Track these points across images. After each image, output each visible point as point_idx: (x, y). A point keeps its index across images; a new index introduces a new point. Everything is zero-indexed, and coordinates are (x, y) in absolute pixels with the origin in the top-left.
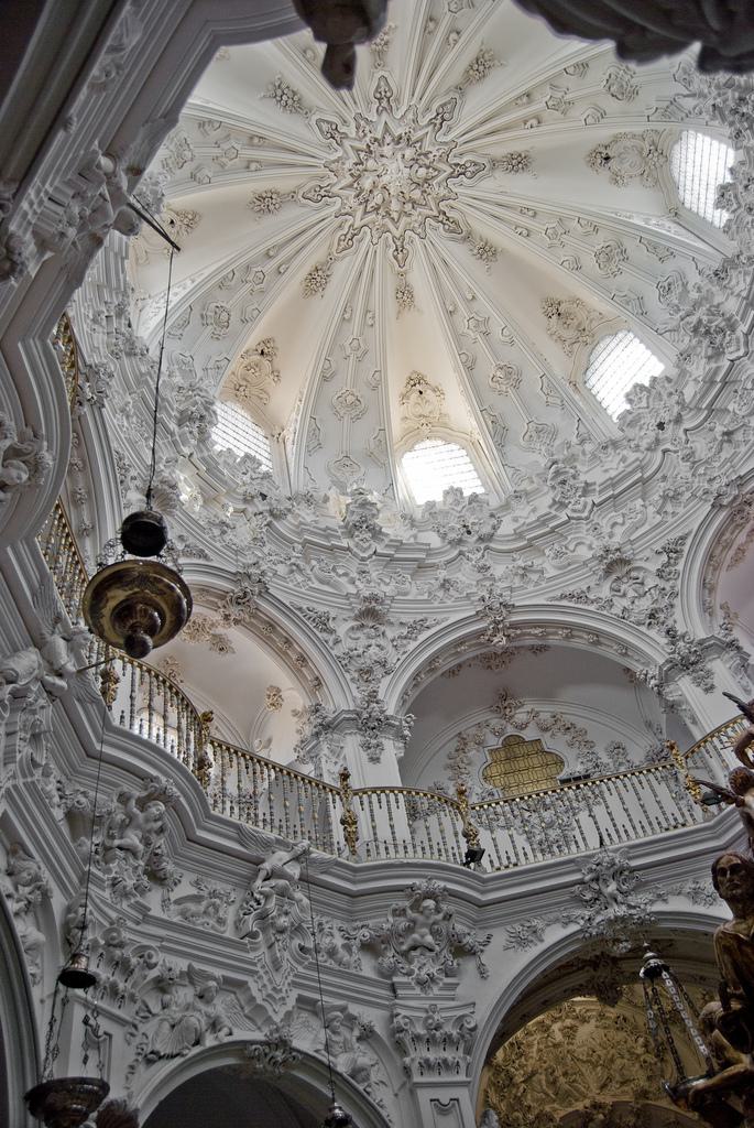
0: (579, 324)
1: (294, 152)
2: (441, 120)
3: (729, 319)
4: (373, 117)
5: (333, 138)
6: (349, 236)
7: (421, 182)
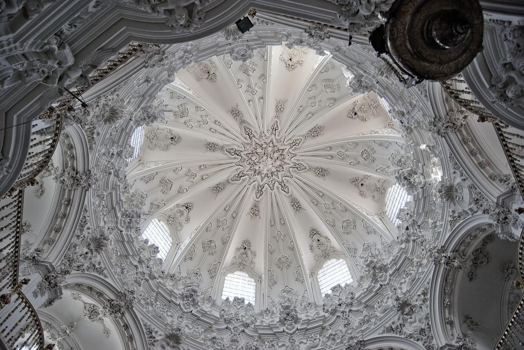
2: (239, 176)
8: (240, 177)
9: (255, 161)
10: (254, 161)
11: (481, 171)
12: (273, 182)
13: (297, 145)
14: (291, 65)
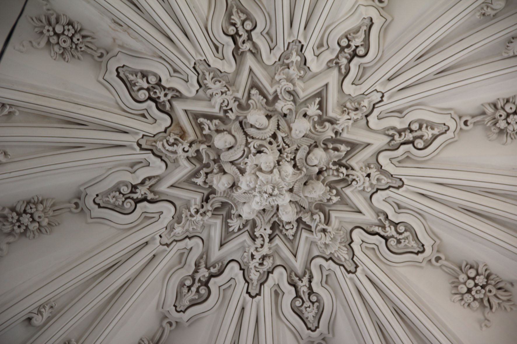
1: (81, 124)
5: (310, 288)
7: (235, 127)
8: (137, 201)
9: (226, 157)
10: (218, 152)
11: (151, 134)
12: (268, 264)
13: (420, 143)
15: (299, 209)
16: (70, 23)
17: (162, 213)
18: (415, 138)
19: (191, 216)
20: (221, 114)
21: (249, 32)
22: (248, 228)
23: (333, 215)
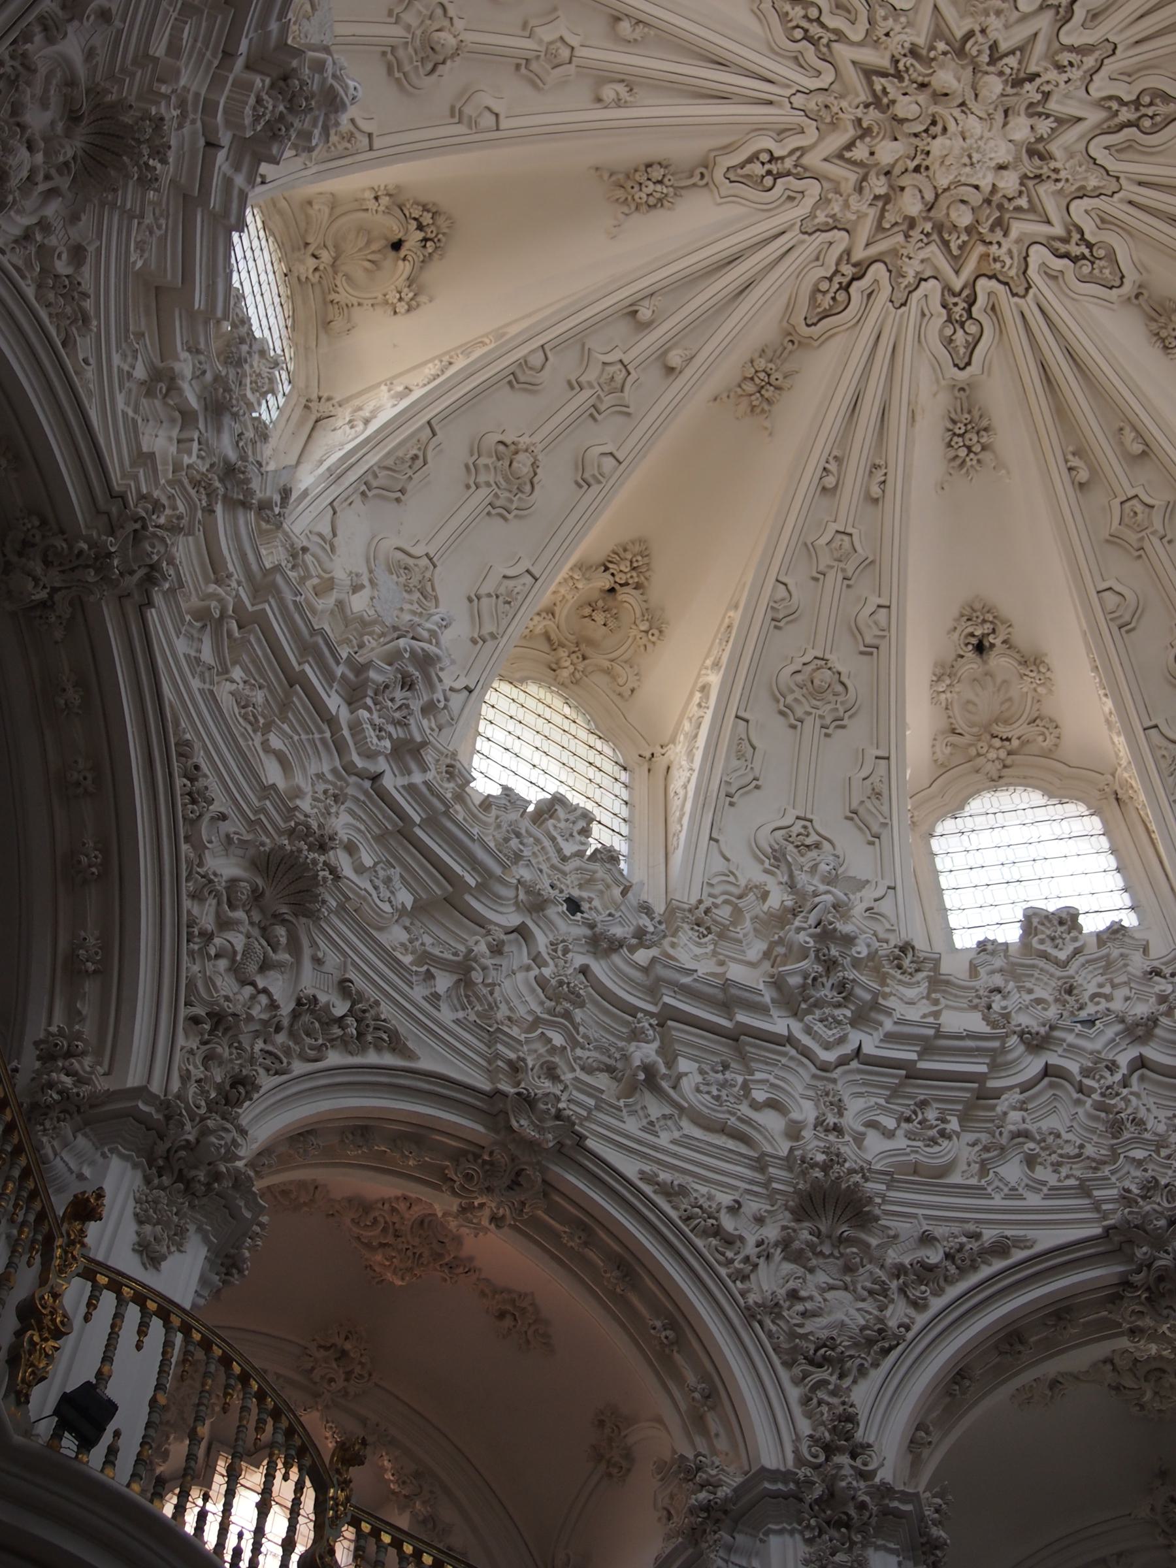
0: (591, 643)
1: (1043, 367)
3: (875, 1006)
4: (1101, 87)
6: (815, 30)
7: (938, 214)
8: (1090, 246)
13: (814, 14)
14: (420, 235)
15: (980, 75)
16: (949, 445)
17: (1086, 212)
18: (810, 20)
19: (1067, 180)
20: (935, 237)
21: (830, 279)
22: (1040, 109)
23: (959, 34)
